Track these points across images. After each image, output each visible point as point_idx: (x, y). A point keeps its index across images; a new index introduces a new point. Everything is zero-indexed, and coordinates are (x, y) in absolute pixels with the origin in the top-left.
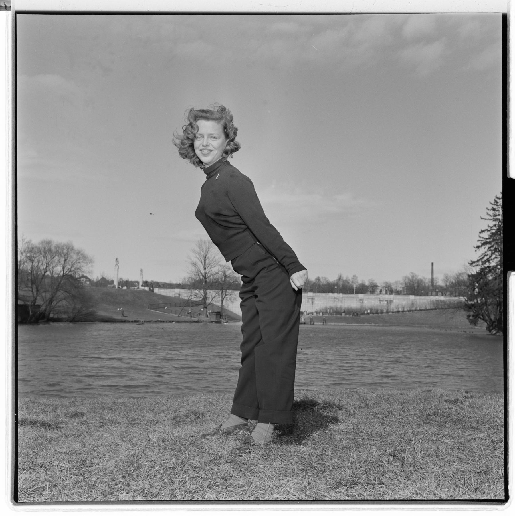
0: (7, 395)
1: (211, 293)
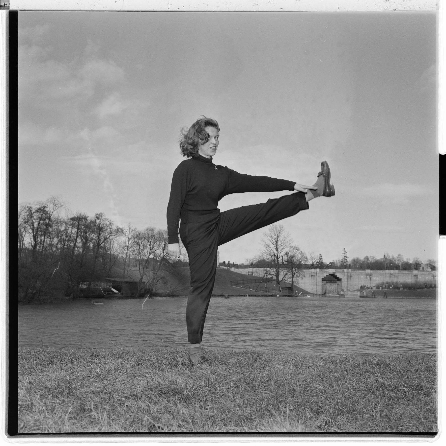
0: (2, 342)
1: (283, 272)
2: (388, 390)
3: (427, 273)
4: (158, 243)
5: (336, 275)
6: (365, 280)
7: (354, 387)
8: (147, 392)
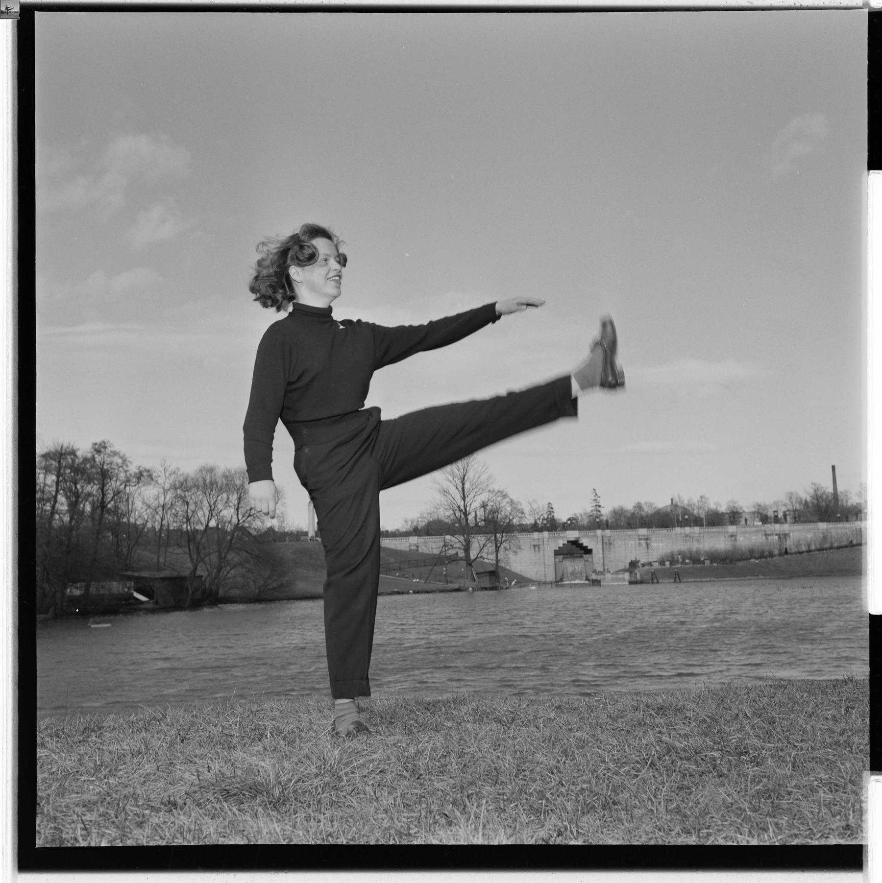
1: (478, 541)
2: (681, 759)
3: (755, 529)
4: (225, 496)
5: (580, 542)
6: (638, 548)
7: (616, 757)
8: (198, 795)
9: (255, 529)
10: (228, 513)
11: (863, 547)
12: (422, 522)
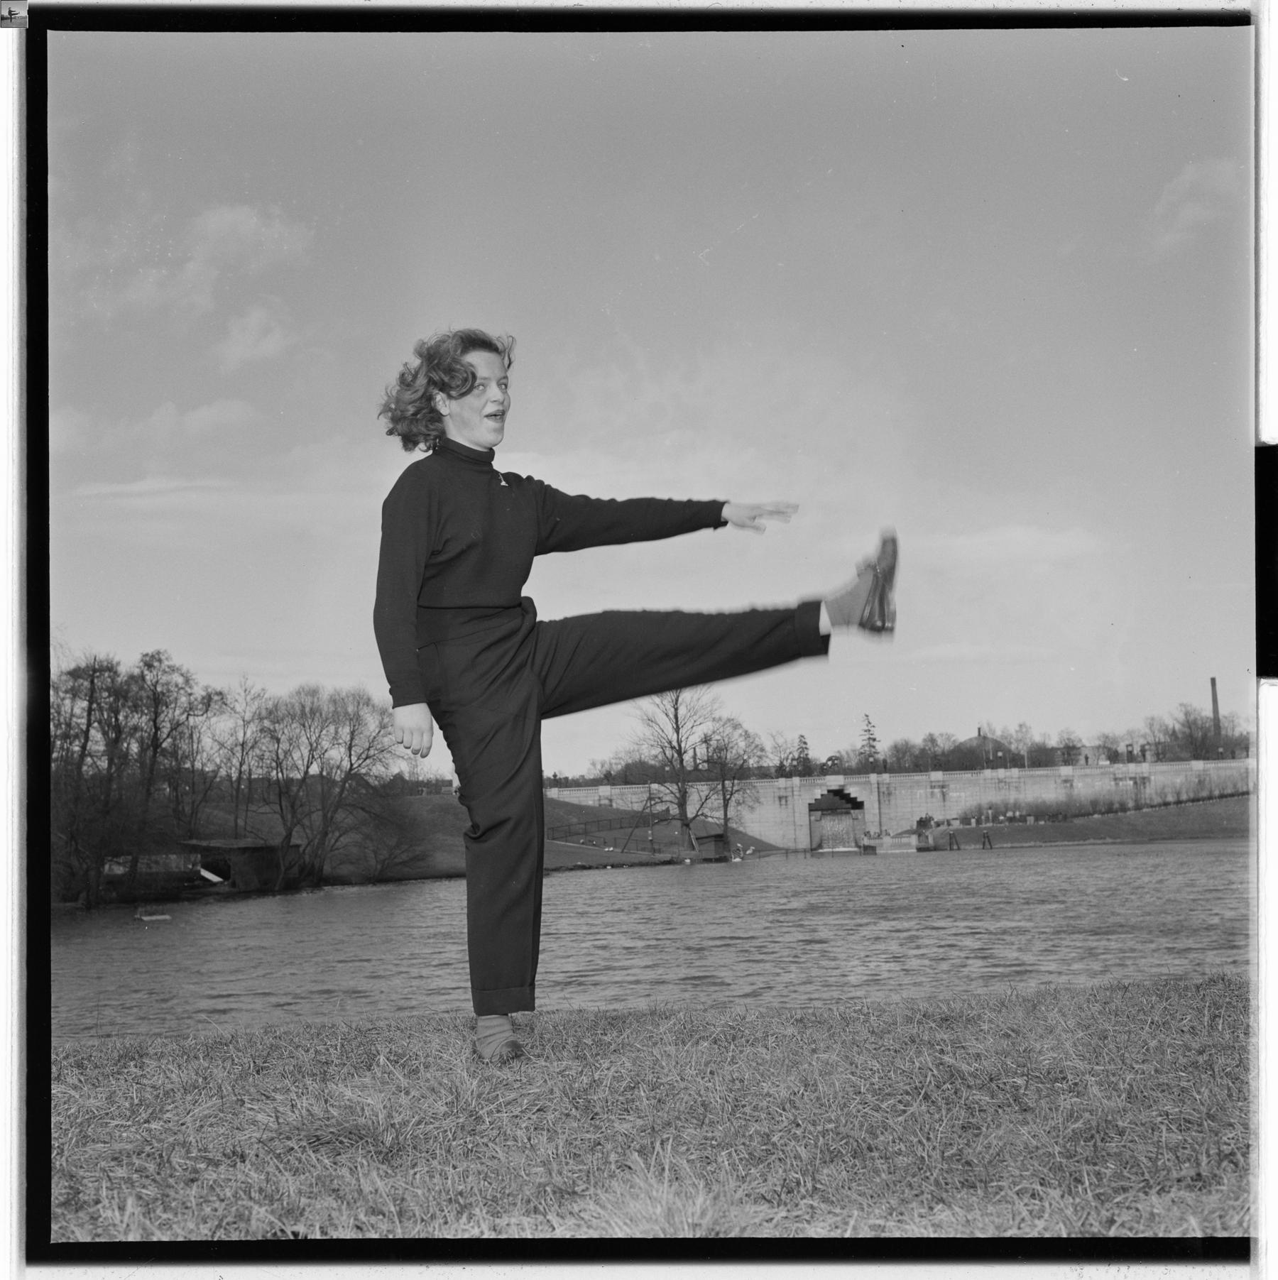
1: (698, 792)
2: (969, 1087)
3: (1098, 771)
4: (332, 728)
9: (376, 777)
10: (337, 754)
11: (1252, 797)
12: (616, 764)
